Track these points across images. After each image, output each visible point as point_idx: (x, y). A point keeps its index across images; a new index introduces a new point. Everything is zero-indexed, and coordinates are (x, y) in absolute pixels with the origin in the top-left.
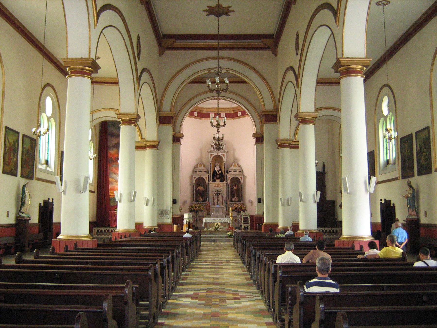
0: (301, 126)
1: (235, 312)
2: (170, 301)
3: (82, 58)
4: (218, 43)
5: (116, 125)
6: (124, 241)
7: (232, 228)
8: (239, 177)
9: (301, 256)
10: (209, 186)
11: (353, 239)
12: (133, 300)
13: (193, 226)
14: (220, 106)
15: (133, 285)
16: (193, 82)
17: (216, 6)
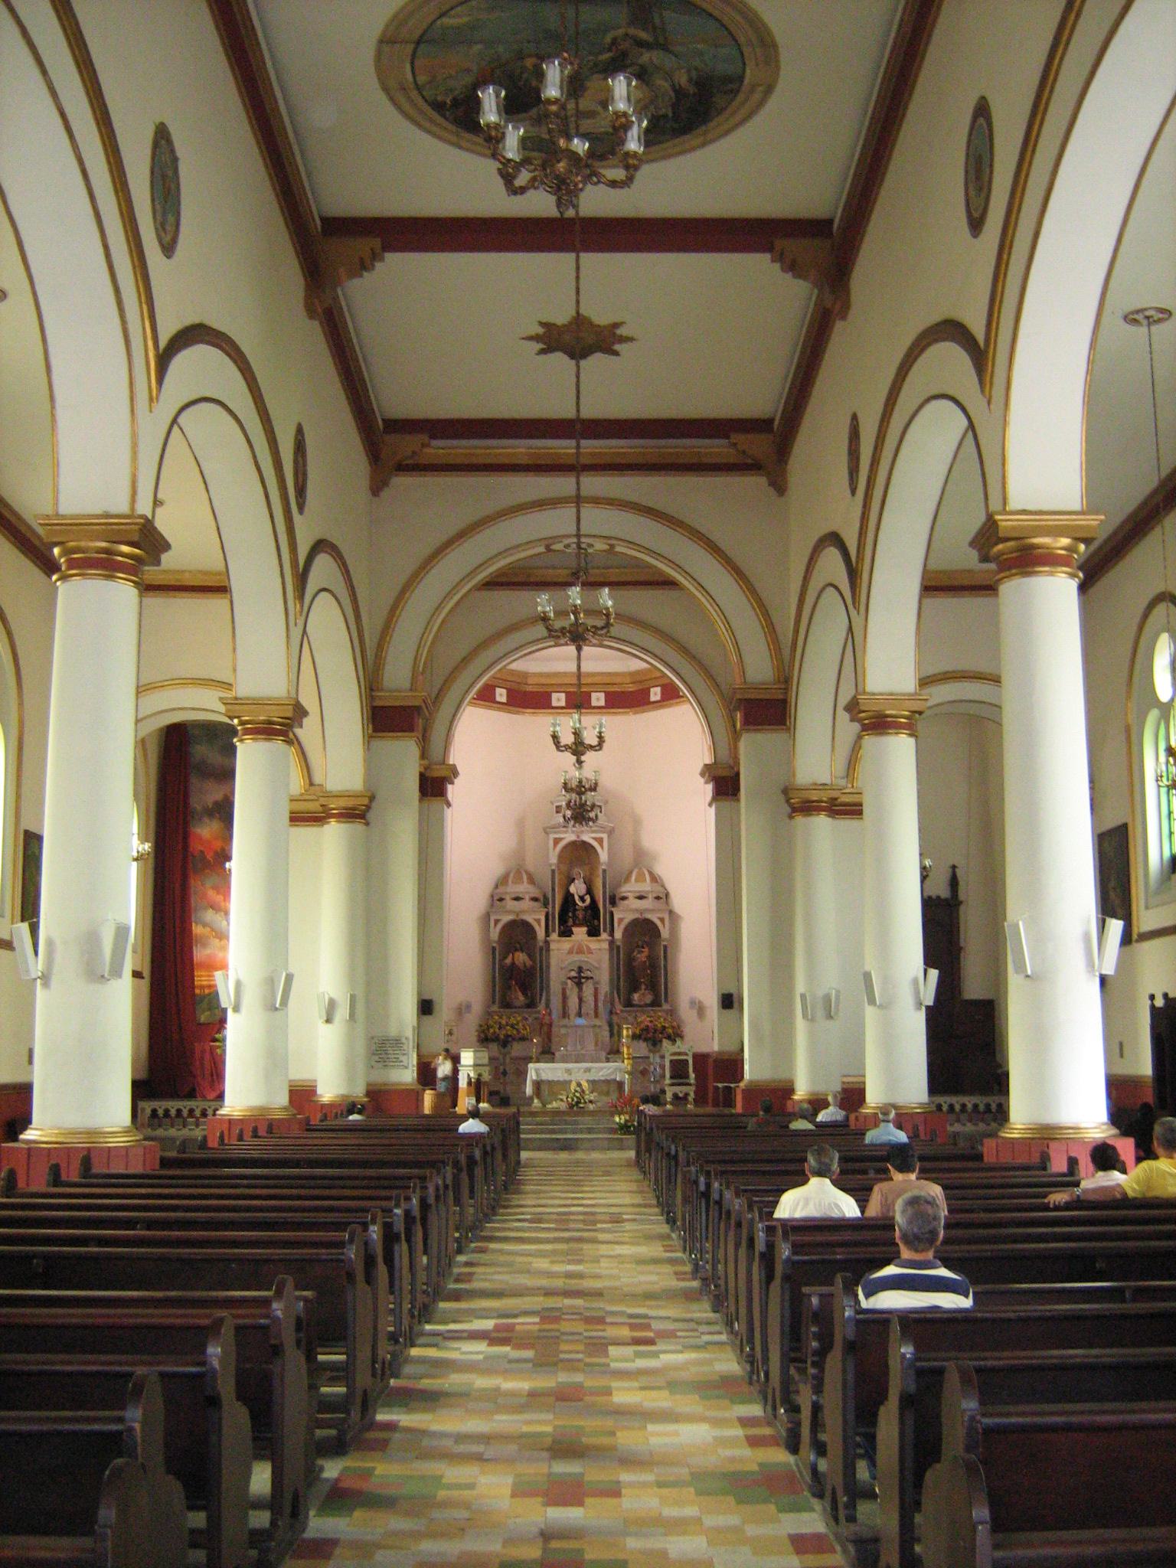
0: (870, 742)
1: (636, 1384)
2: (414, 1352)
3: (108, 516)
4: (578, 447)
5: (221, 737)
6: (250, 1148)
7: (631, 1100)
8: (654, 918)
9: (861, 1195)
10: (548, 950)
11: (1046, 1136)
12: (298, 1343)
13: (491, 1094)
14: (587, 667)
15: (297, 1293)
16: (493, 584)
17: (570, 323)
